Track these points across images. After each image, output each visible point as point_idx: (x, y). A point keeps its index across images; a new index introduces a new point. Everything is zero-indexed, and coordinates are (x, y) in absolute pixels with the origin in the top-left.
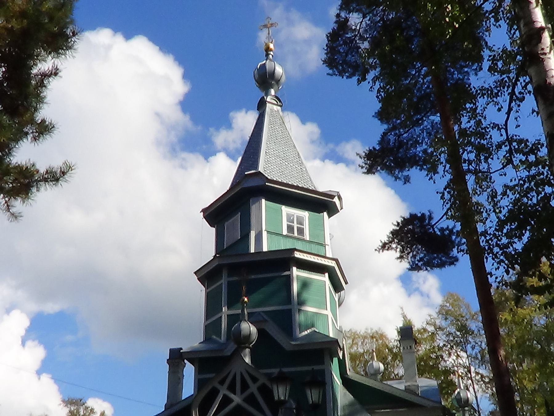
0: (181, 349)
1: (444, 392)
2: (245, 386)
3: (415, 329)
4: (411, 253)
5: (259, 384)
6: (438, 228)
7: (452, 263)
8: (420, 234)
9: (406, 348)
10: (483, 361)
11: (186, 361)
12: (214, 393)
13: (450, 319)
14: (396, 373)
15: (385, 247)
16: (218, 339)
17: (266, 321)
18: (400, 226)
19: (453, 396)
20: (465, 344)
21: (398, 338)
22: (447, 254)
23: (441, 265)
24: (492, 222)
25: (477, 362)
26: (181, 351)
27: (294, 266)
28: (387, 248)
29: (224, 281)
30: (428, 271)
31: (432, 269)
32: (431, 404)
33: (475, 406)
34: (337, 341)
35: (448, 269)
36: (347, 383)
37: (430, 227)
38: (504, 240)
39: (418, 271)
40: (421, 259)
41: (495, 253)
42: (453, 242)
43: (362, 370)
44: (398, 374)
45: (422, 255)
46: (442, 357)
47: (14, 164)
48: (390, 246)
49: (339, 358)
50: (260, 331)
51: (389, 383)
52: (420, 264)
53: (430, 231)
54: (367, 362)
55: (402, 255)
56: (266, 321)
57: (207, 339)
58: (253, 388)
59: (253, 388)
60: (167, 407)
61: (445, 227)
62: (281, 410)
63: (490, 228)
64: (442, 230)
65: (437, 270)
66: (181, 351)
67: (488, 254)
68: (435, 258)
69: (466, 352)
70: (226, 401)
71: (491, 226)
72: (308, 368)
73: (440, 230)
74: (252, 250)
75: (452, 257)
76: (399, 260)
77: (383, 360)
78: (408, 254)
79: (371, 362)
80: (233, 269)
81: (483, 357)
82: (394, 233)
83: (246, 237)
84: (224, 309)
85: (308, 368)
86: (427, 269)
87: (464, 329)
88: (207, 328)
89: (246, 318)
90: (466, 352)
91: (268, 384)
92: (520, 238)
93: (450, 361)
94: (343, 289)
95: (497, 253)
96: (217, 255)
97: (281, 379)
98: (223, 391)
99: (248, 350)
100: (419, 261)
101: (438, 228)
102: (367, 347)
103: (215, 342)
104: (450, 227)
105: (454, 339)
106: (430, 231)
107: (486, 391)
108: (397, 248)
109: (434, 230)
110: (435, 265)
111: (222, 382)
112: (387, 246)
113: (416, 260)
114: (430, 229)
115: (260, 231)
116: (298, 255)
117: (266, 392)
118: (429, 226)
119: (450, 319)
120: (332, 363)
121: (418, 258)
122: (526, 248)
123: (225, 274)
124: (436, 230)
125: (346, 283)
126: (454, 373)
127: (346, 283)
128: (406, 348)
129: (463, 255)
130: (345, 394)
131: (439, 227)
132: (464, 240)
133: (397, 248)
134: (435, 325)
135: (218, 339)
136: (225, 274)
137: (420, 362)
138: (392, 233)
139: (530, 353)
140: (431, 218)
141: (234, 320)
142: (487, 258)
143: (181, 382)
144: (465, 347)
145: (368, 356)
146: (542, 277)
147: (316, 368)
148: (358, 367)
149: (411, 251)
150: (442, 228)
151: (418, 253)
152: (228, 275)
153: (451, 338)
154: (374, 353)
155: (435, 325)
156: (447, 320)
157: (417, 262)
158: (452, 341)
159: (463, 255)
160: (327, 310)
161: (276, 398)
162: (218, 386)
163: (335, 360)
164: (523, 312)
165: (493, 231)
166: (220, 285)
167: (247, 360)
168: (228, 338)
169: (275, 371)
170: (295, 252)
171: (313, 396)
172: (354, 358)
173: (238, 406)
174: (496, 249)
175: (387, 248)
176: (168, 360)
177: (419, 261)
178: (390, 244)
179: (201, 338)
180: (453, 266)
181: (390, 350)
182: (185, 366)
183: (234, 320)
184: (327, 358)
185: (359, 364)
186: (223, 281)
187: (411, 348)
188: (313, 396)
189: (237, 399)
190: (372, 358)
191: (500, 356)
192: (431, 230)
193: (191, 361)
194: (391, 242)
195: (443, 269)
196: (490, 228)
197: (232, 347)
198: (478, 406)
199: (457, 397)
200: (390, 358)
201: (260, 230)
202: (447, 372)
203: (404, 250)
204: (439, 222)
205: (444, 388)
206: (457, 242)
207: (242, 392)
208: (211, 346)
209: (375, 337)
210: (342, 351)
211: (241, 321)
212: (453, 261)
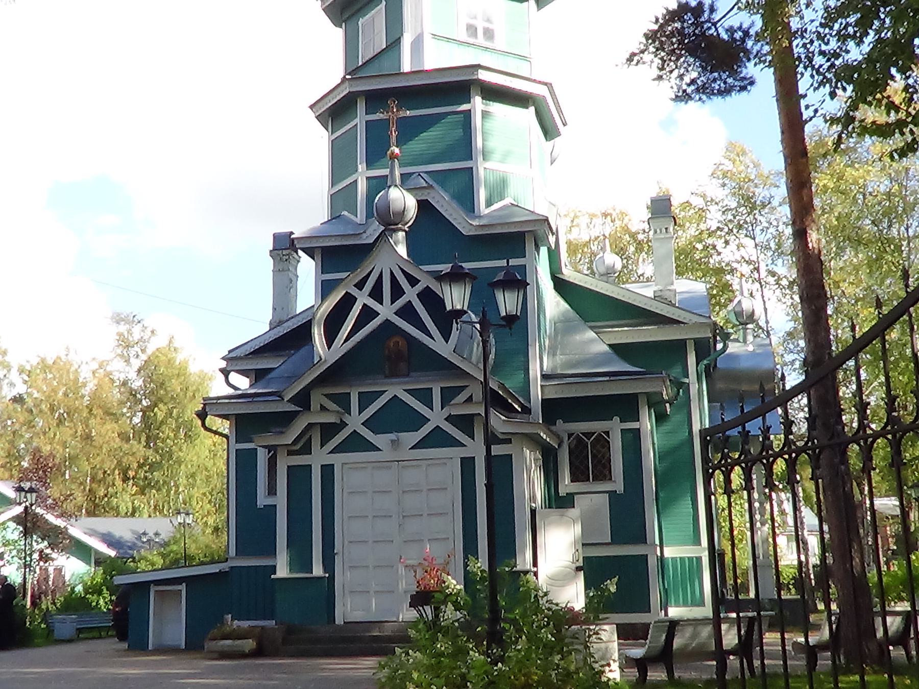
0: (292, 233)
1: (713, 301)
2: (397, 291)
3: (675, 202)
4: (677, 71)
5: (419, 287)
6: (723, 27)
7: (743, 88)
8: (694, 38)
9: (658, 231)
10: (779, 251)
11: (300, 252)
12: (348, 301)
13: (729, 186)
14: (640, 272)
15: (633, 60)
16: (352, 217)
17: (430, 187)
18: (659, 24)
19: (730, 308)
20: (752, 226)
21: (646, 215)
22: (734, 73)
23: (725, 92)
24: (817, 11)
25: (770, 253)
26: (293, 236)
27: (477, 95)
28: (635, 62)
29: (360, 119)
30: (703, 102)
31: (710, 98)
32: (696, 319)
33: (762, 323)
34: (546, 220)
35: (736, 98)
36: (562, 286)
37: (710, 25)
38: (833, 44)
39: (686, 102)
40: (693, 82)
41: (816, 67)
42: (747, 52)
43: (586, 268)
44: (642, 275)
45: (694, 75)
46: (714, 247)
47: (151, 534)
48: (641, 58)
49: (549, 249)
50: (423, 205)
51: (628, 286)
52: (689, 90)
53: (711, 32)
54: (593, 254)
55: (661, 74)
56: (430, 187)
57: (335, 217)
58: (411, 294)
59: (411, 294)
60: (273, 326)
61: (736, 25)
62: (457, 323)
63: (812, 21)
64: (731, 30)
65: (717, 100)
66: (293, 236)
67: (806, 68)
68: (715, 80)
69: (754, 239)
70: (367, 314)
71: (813, 18)
72: (503, 263)
73: (727, 31)
74: (406, 67)
75: (744, 78)
76: (657, 82)
77: (621, 252)
78: (671, 72)
79: (601, 254)
80: (376, 99)
81: (779, 245)
82: (651, 36)
83: (394, 44)
84: (361, 167)
85: (503, 263)
86: (700, 99)
87: (750, 203)
88: (333, 197)
89: (398, 182)
90: (754, 239)
91: (435, 286)
92: (860, 43)
93: (728, 254)
94: (559, 134)
95: (821, 66)
96: (348, 77)
97: (456, 276)
98: (363, 299)
99: (401, 235)
100: (689, 85)
101: (723, 27)
102: (595, 233)
103: (349, 222)
104: (745, 26)
105: (735, 218)
106: (711, 32)
107: (784, 300)
108: (652, 62)
109: (716, 29)
110: (715, 91)
111: (360, 285)
112: (636, 58)
113: (684, 82)
114: (709, 28)
115: (419, 35)
116: (483, 75)
117: (430, 299)
118: (710, 22)
119: (729, 186)
120: (538, 255)
121: (687, 79)
122: (869, 59)
123: (361, 106)
124: (720, 30)
125: (565, 124)
126: (733, 271)
127: (565, 124)
128: (658, 231)
129: (762, 69)
130: (558, 304)
131: (726, 25)
132: (766, 48)
133: (652, 62)
134: (704, 196)
135: (352, 217)
136: (361, 106)
137: (680, 254)
138: (646, 35)
139: (858, 242)
140: (712, 10)
141: (378, 185)
142: (802, 74)
143: (294, 286)
144: (753, 230)
145: (596, 246)
146: (892, 106)
147: (513, 262)
148: (581, 262)
149: (676, 67)
150: (732, 27)
151: (688, 71)
152: (290, 570)
153: (730, 217)
154: (607, 241)
155: (704, 196)
156: (725, 188)
157: (685, 87)
158: (730, 221)
159: (762, 69)
160: (429, 420)
161: (449, 307)
162: (354, 292)
163: (544, 250)
164: (853, 173)
165: (817, 27)
166: (353, 127)
167: (402, 250)
168: (369, 215)
169: (445, 268)
170: (480, 71)
171: (507, 302)
172: (573, 248)
173: (387, 322)
174: (818, 60)
175: (635, 62)
176: (271, 251)
177: (689, 85)
178: (641, 55)
179: (325, 216)
180: (744, 93)
181: (633, 236)
182: (299, 261)
183: (378, 185)
184: (530, 246)
185: (580, 259)
186: (357, 120)
187: (666, 232)
188: (507, 302)
189: (386, 311)
190: (603, 249)
191: (811, 241)
192: (712, 31)
193: (310, 252)
194: (642, 52)
195: (728, 98)
196: (812, 21)
197: (376, 228)
198: (767, 322)
199: (736, 310)
200: (632, 249)
201: (419, 31)
202: (719, 271)
203: (663, 66)
204: (728, 16)
205: (714, 296)
206: (755, 52)
207: (395, 297)
208: (339, 229)
209: (611, 215)
210: (554, 236)
211: (390, 187)
212: (747, 84)
